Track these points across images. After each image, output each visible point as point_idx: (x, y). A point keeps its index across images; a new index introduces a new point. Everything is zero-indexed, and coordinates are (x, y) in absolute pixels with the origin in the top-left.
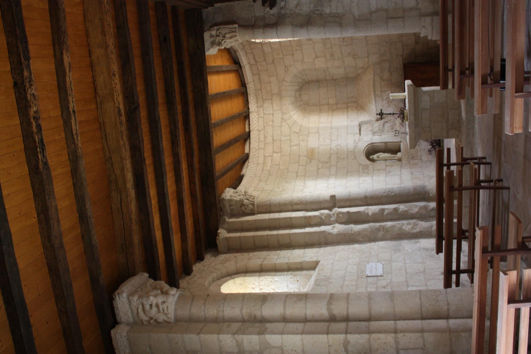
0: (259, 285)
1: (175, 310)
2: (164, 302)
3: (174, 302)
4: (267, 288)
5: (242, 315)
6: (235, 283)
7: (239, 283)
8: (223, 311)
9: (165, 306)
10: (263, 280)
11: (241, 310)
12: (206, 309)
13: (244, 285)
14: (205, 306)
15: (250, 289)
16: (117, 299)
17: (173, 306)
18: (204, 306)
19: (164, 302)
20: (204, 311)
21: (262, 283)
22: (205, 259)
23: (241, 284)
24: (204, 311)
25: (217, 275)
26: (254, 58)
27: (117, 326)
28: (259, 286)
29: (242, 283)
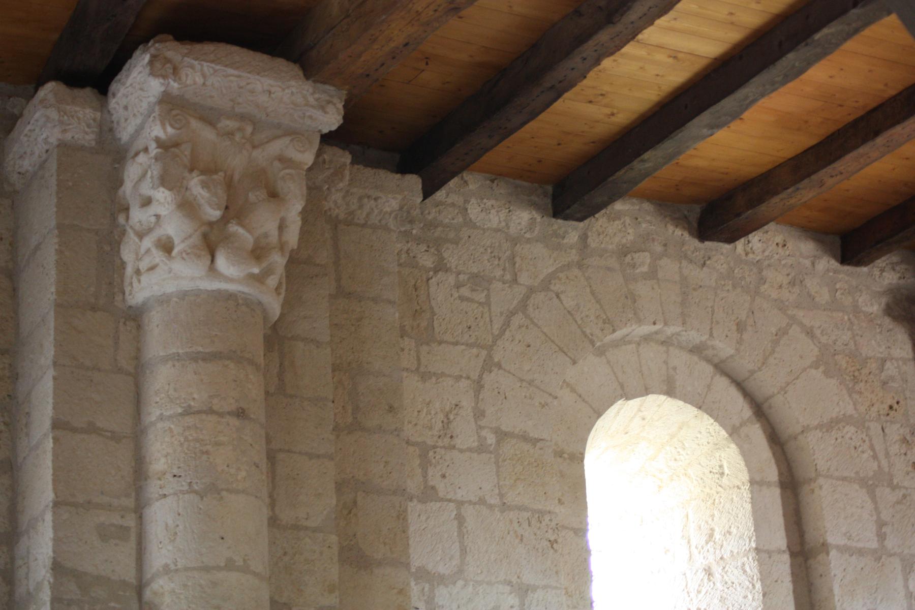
0: (725, 557)
1: (164, 300)
2: (167, 247)
3: (186, 285)
4: (716, 601)
5: (153, 579)
6: (717, 447)
7: (721, 466)
8: (165, 496)
9: (158, 256)
10: (745, 572)
11: (166, 570)
12: (167, 424)
13: (720, 489)
14: (181, 414)
15: (707, 522)
16: (144, 59)
17: (171, 288)
18: (180, 410)
19: (167, 247)
20: (161, 418)
21: (735, 575)
22: (865, 269)
23: (722, 474)
24: (161, 418)
25: (732, 356)
26: (617, 378)
27: (88, 92)
28: (722, 558)
29: (725, 480)
